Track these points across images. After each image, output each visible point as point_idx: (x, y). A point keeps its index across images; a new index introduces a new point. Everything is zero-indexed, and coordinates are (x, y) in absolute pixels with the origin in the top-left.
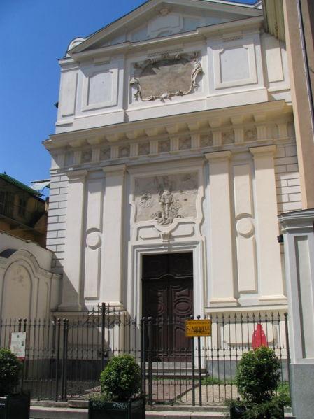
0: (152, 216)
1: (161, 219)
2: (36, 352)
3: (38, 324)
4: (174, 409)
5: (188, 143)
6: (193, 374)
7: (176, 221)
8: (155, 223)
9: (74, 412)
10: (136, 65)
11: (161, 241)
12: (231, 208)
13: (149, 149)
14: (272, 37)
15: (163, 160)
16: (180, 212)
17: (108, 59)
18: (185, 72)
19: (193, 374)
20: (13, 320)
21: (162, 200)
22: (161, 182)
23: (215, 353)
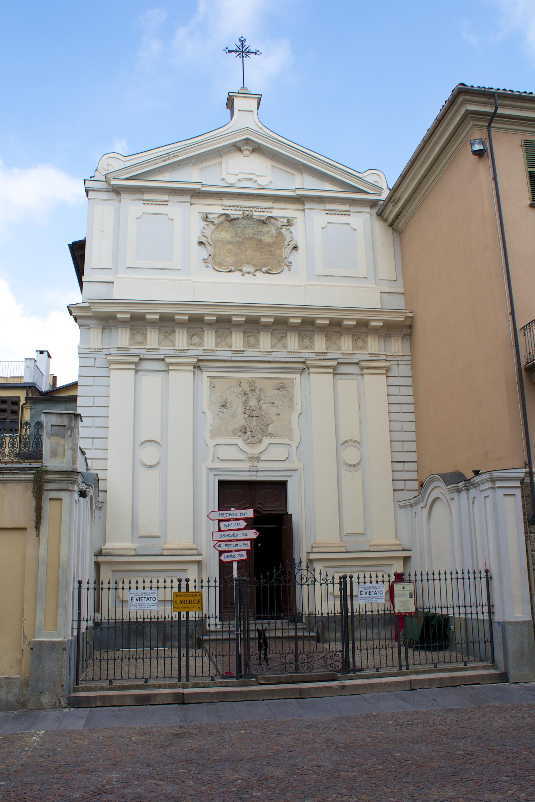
0: (234, 433)
1: (245, 437)
2: (468, 609)
3: (466, 575)
4: (359, 678)
5: (282, 341)
6: (296, 633)
7: (266, 441)
8: (239, 441)
9: (202, 693)
10: (206, 218)
11: (246, 465)
12: (529, 448)
13: (231, 343)
14: (383, 223)
15: (276, 359)
16: (270, 430)
17: (165, 197)
18: (274, 243)
19: (296, 633)
20: (442, 573)
21: (248, 412)
22: (246, 386)
23: (462, 610)
